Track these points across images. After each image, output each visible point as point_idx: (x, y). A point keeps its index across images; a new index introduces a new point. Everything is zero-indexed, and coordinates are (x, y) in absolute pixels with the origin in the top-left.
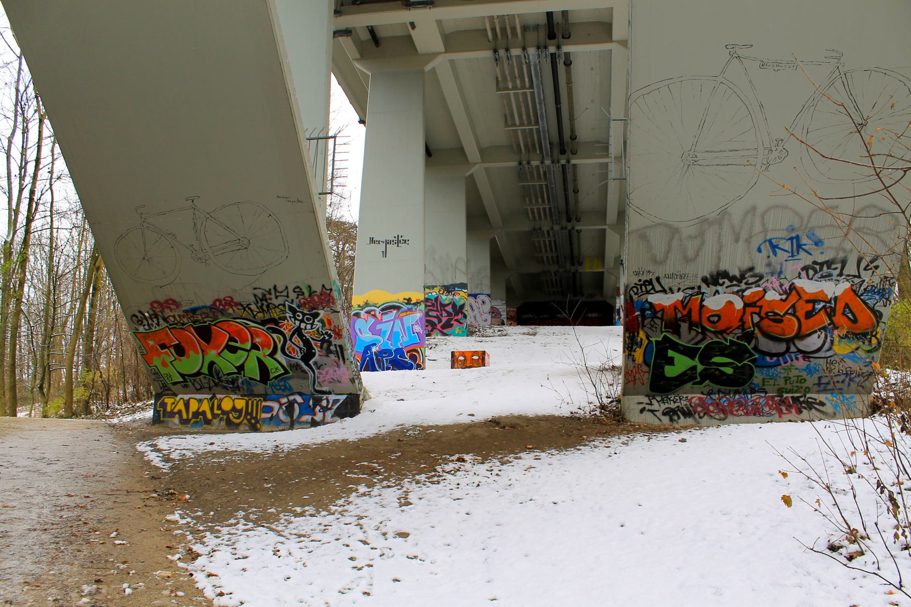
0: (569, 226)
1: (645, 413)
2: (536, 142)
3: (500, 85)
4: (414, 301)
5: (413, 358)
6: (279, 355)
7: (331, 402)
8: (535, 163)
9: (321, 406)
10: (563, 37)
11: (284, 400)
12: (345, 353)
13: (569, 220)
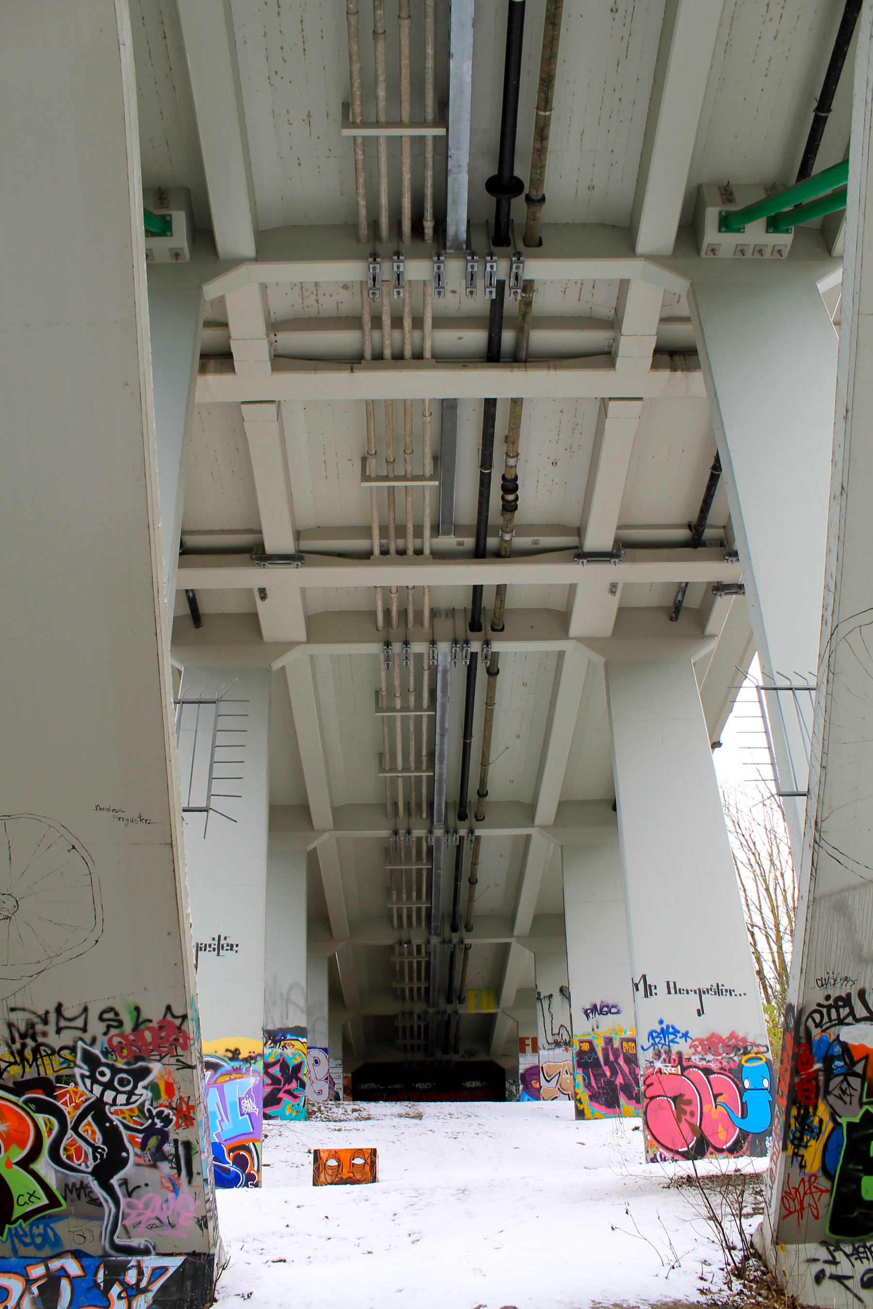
0: (455, 938)
1: (826, 1283)
2: (424, 798)
3: (380, 700)
4: (244, 1054)
5: (241, 1162)
6: (44, 1166)
7: (147, 1273)
8: (419, 832)
9: (123, 1283)
10: (493, 629)
11: (37, 1271)
12: (195, 1159)
13: (454, 929)
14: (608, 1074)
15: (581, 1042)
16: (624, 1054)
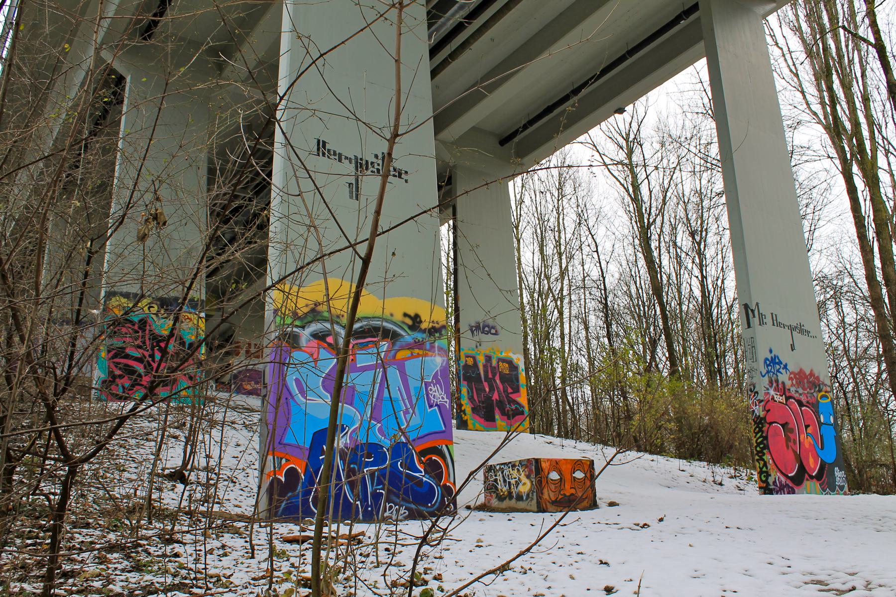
14: (487, 389)
15: (467, 356)
16: (500, 373)
